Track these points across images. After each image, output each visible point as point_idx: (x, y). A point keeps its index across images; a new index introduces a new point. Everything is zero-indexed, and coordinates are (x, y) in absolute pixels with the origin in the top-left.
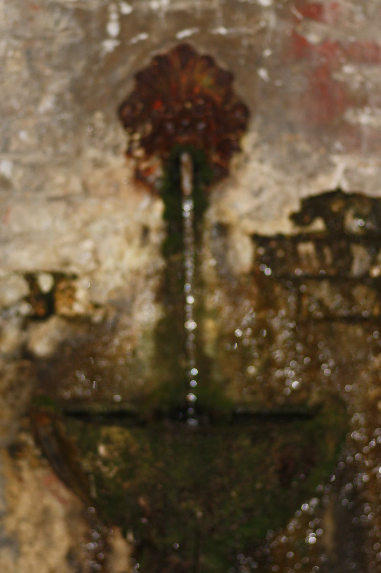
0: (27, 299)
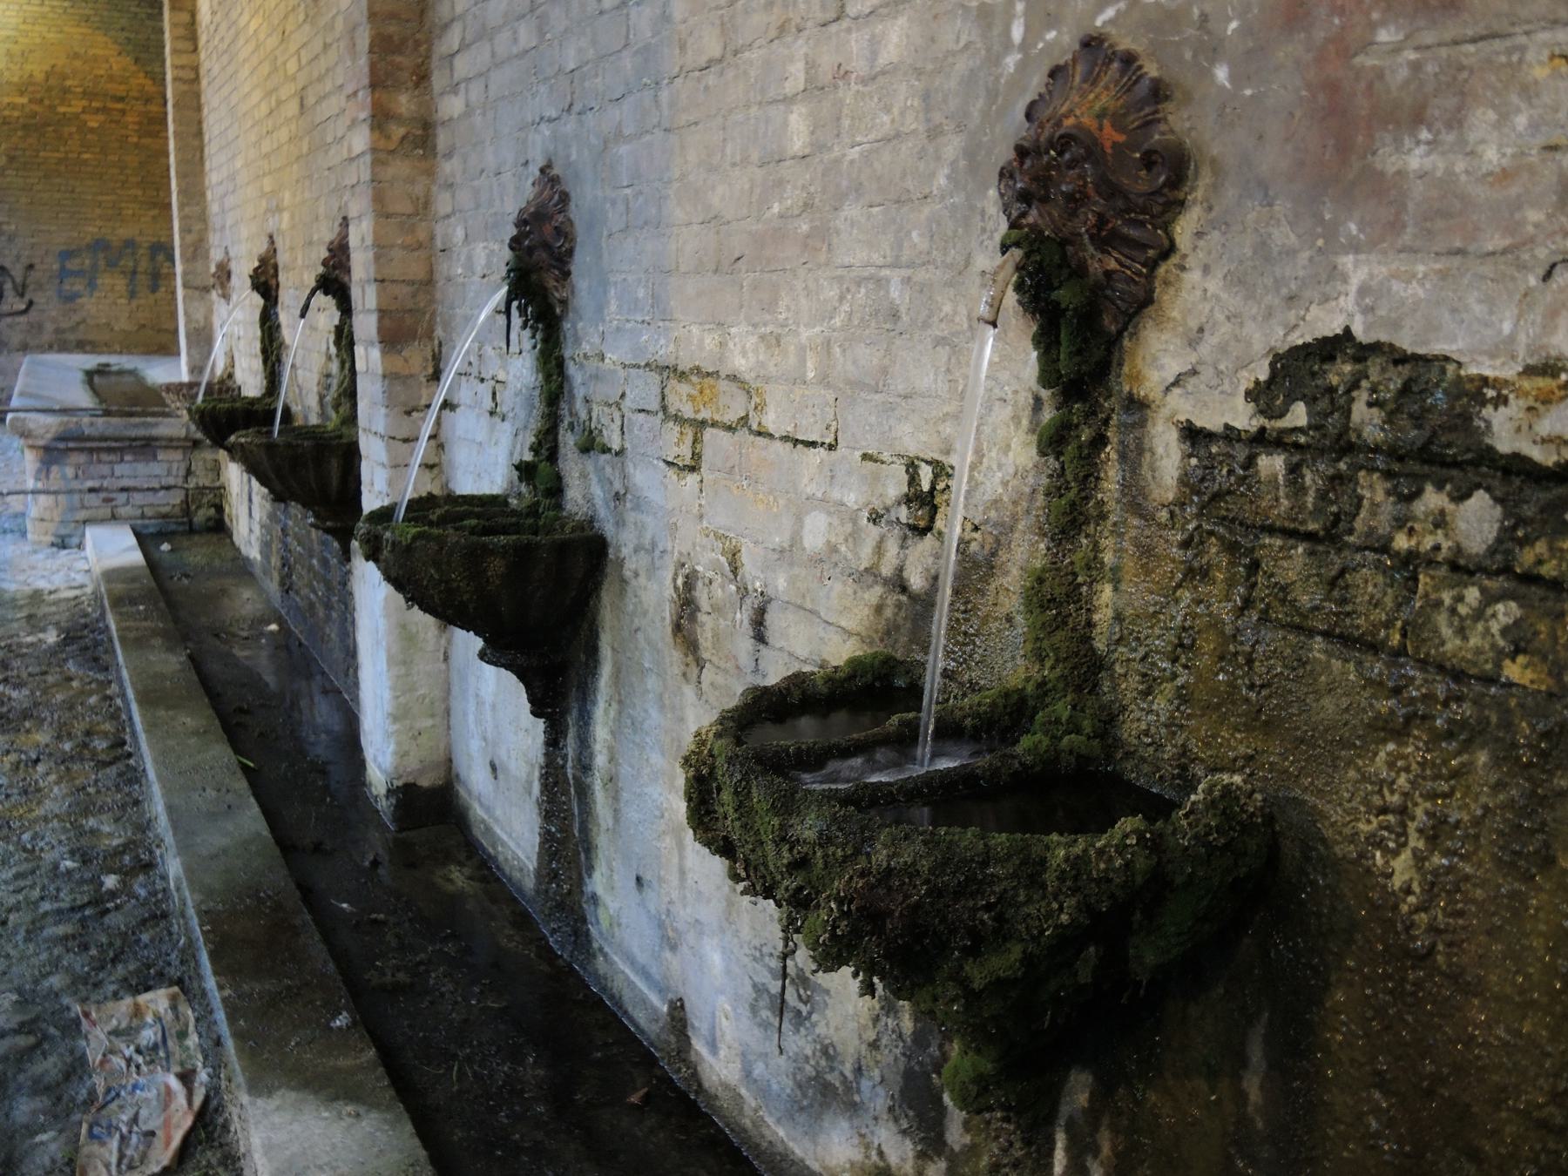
0: (908, 500)
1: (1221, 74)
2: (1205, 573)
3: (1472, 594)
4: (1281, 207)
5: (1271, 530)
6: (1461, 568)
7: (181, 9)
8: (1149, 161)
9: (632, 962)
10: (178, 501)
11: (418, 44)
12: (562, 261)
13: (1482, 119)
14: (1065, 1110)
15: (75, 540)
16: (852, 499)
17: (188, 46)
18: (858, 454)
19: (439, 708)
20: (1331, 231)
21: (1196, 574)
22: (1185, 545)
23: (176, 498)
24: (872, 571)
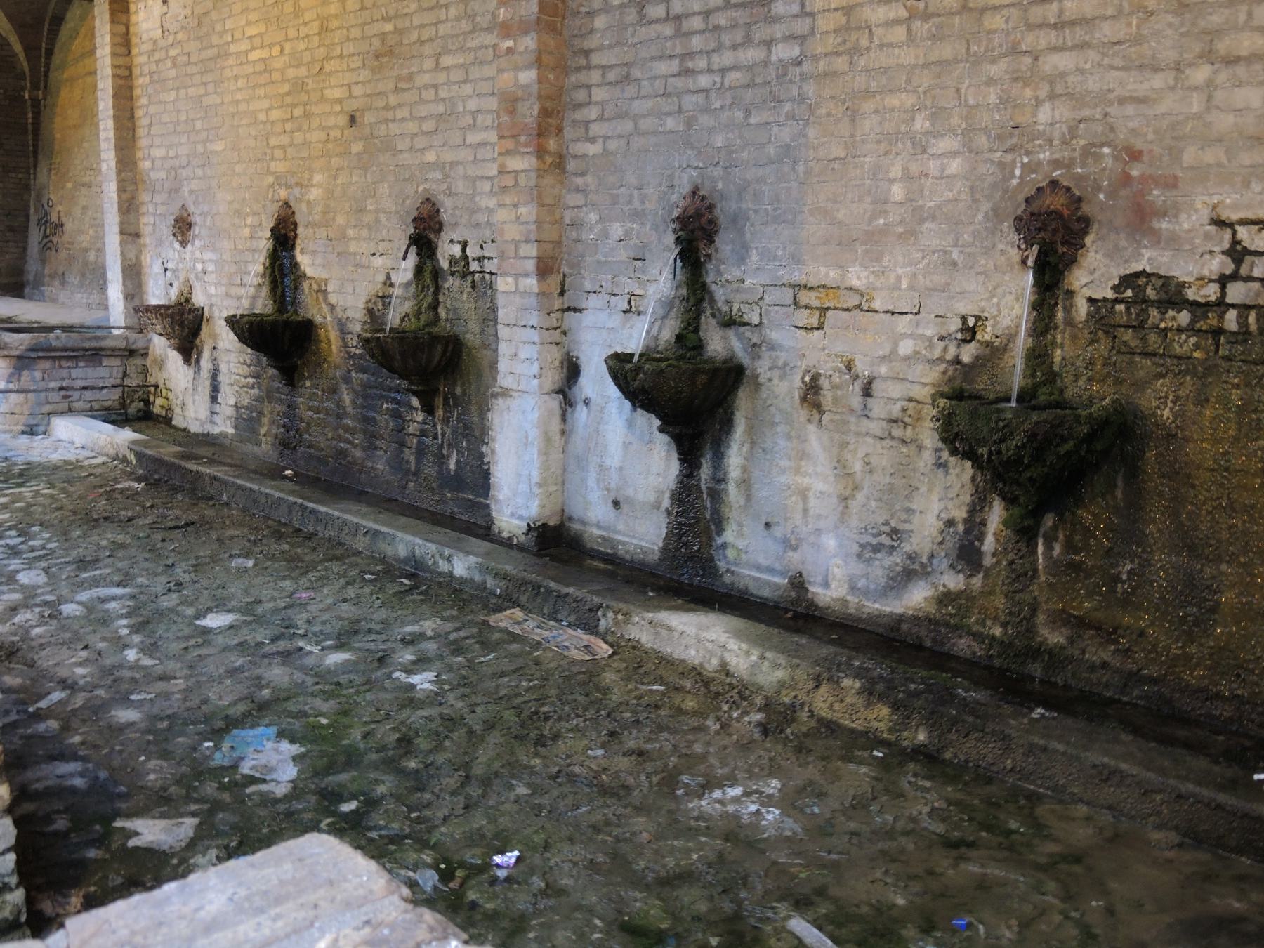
0: (962, 330)
1: (1102, 196)
2: (1097, 341)
3: (1184, 337)
4: (1122, 235)
5: (1120, 326)
6: (1180, 330)
8: (1079, 219)
9: (759, 568)
11: (559, 112)
13: (1183, 216)
14: (1042, 530)
15: (41, 429)
16: (929, 333)
17: (123, 50)
19: (560, 479)
20: (1139, 243)
21: (1092, 342)
23: (116, 394)
24: (941, 359)
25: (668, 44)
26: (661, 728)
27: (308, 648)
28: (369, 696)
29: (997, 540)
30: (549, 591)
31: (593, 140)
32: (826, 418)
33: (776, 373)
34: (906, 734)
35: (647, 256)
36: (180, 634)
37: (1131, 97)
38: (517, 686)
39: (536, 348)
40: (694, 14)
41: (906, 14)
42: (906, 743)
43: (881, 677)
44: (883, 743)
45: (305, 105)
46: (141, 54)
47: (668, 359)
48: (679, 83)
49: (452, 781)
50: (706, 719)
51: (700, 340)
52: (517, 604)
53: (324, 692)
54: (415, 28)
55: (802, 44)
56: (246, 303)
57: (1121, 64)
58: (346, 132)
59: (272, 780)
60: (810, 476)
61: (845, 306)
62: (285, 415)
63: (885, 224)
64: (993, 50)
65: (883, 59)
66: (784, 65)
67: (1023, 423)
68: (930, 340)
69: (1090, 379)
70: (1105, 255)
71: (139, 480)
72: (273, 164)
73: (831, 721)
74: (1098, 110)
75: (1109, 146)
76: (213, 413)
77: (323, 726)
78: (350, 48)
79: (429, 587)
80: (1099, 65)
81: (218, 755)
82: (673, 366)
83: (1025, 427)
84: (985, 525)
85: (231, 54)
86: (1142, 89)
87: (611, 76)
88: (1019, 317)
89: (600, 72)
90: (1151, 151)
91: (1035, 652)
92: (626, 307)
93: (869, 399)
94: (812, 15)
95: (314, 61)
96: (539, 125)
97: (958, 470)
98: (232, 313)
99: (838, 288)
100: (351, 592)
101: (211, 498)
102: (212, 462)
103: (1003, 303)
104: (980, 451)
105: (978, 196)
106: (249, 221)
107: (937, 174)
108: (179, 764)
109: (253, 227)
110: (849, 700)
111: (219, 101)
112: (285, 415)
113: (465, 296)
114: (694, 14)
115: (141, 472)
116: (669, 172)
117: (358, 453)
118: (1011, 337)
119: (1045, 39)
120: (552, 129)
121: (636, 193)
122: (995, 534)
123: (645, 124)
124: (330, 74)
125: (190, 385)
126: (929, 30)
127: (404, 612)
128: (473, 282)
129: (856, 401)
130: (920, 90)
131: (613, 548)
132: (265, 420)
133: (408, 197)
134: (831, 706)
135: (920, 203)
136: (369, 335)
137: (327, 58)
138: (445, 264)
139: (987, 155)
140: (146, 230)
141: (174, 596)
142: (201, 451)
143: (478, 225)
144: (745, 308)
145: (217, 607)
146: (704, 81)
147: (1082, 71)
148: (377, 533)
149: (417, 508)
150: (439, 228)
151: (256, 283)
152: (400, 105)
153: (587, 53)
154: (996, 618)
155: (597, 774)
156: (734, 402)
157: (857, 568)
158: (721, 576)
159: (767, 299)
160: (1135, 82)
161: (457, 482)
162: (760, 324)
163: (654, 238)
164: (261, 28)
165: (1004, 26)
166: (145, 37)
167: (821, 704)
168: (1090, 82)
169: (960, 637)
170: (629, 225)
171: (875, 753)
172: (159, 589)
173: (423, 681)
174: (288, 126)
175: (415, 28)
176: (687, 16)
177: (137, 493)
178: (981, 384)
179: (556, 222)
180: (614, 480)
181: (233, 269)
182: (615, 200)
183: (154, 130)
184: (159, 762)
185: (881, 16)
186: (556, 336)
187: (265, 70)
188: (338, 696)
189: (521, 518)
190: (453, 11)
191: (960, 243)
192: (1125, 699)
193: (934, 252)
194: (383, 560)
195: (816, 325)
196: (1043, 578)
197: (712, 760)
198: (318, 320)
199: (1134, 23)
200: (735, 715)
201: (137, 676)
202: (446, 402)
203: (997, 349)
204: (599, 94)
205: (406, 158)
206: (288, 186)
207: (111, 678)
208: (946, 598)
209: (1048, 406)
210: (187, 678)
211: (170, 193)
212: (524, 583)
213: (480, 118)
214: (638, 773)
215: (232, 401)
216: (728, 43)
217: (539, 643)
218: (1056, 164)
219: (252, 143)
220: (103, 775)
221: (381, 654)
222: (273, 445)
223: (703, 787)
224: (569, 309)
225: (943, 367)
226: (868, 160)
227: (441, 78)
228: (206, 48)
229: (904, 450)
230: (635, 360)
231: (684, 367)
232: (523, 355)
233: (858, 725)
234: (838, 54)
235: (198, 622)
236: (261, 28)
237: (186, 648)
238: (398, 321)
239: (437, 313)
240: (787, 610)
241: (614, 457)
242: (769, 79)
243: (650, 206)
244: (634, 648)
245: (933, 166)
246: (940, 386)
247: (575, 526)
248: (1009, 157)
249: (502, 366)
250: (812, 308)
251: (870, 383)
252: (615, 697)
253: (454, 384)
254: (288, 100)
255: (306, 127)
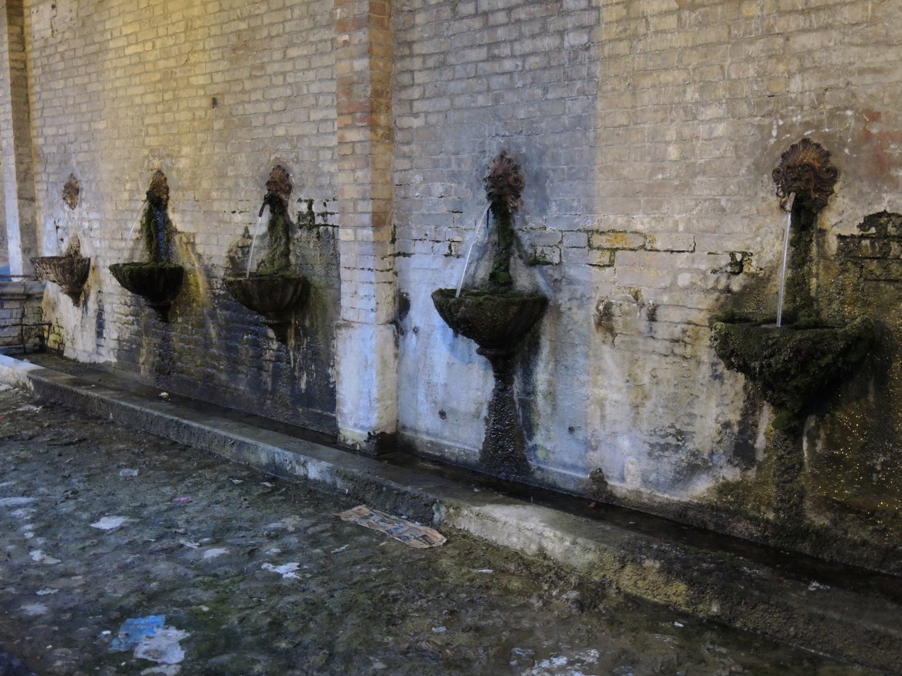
0: (731, 264)
1: (846, 151)
2: (847, 271)
4: (865, 183)
5: (866, 258)
7: (14, 25)
8: (828, 170)
9: (565, 466)
10: (16, 334)
11: (387, 93)
12: (516, 190)
14: (806, 430)
16: (703, 267)
17: (18, 47)
18: (706, 253)
21: (843, 271)
22: (841, 264)
23: (16, 332)
24: (714, 289)
25: (478, 35)
26: (493, 607)
27: (188, 545)
28: (242, 586)
29: (767, 438)
30: (390, 490)
31: (416, 115)
32: (618, 340)
33: (575, 303)
34: (701, 607)
35: (464, 209)
36: (78, 536)
37: (869, 69)
38: (367, 573)
39: (374, 287)
40: (499, 10)
41: (676, 6)
42: (701, 615)
43: (677, 558)
44: (682, 615)
45: (174, 90)
46: (34, 50)
47: (483, 294)
48: (488, 67)
49: (318, 659)
50: (530, 597)
51: (510, 277)
52: (364, 502)
53: (204, 583)
54: (266, 26)
55: (589, 33)
56: (126, 254)
57: (860, 41)
58: (209, 112)
59: (163, 663)
60: (606, 388)
61: (631, 247)
62: (161, 346)
63: (663, 179)
64: (750, 33)
65: (659, 43)
66: (575, 51)
67: (789, 341)
68: (704, 273)
69: (842, 303)
70: (852, 200)
71: (37, 404)
72: (147, 140)
73: (636, 596)
74: (842, 79)
75: (852, 109)
76: (98, 345)
77: (204, 613)
78: (211, 43)
79: (288, 488)
80: (841, 43)
81: (115, 642)
82: (490, 300)
83: (790, 344)
84: (757, 426)
85: (111, 50)
86: (878, 62)
87: (431, 62)
88: (781, 253)
89: (421, 59)
90: (887, 112)
91: (805, 533)
92: (447, 251)
93: (654, 324)
94: (597, 8)
95: (181, 54)
96: (372, 104)
97: (731, 381)
98: (114, 262)
99: (625, 232)
100: (222, 495)
101: (99, 418)
102: (99, 387)
103: (765, 242)
104: (753, 365)
105: (741, 153)
106: (128, 186)
107: (706, 136)
108: (82, 651)
109: (131, 191)
110: (650, 578)
111: (101, 88)
112: (161, 346)
113: (312, 245)
114: (499, 10)
115: (38, 397)
116: (481, 140)
117: (223, 377)
118: (773, 270)
119: (793, 23)
120: (383, 107)
121: (453, 158)
122: (765, 434)
123: (460, 101)
124: (195, 64)
125: (79, 323)
126: (696, 18)
127: (268, 511)
128: (318, 233)
129: (643, 325)
130: (690, 67)
131: (440, 451)
132: (143, 351)
133: (262, 165)
134: (636, 583)
135: (693, 160)
136: (232, 279)
137: (192, 51)
138: (294, 219)
139: (747, 120)
140: (40, 195)
141: (71, 503)
142: (88, 378)
143: (321, 187)
144: (547, 251)
145: (108, 511)
146: (508, 65)
147: (827, 49)
148: (242, 444)
149: (273, 421)
150: (289, 189)
151: (134, 237)
152: (254, 90)
153: (410, 44)
154: (769, 505)
155: (442, 648)
156: (540, 328)
157: (647, 464)
158: (533, 473)
159: (566, 242)
160: (872, 56)
161: (307, 399)
162: (561, 262)
163: (470, 194)
164: (135, 28)
165: (759, 13)
166: (37, 36)
167: (626, 582)
168: (834, 57)
169: (739, 521)
170: (449, 184)
171: (676, 624)
172: (58, 497)
173: (288, 570)
174: (160, 108)
175: (266, 26)
176: (493, 12)
177: (36, 415)
178: (749, 309)
179: (387, 183)
180: (440, 395)
181: (115, 226)
182: (436, 165)
183: (47, 113)
184: (64, 650)
185: (656, 8)
186: (389, 276)
187: (139, 62)
188: (216, 586)
189: (362, 428)
190: (297, 12)
191: (728, 191)
192: (884, 571)
193: (705, 201)
194: (248, 467)
195: (607, 263)
196: (808, 470)
197: (538, 633)
198: (188, 266)
199: (870, 7)
200: (554, 593)
201: (43, 574)
202: (297, 334)
203: (762, 279)
204: (420, 78)
205: (260, 133)
206: (161, 157)
207: (20, 576)
208: (725, 488)
209: (807, 327)
210: (85, 574)
211: (60, 164)
212: (368, 483)
213: (321, 99)
214: (477, 647)
215: (115, 336)
216: (527, 34)
217: (384, 535)
218: (807, 125)
219: (129, 122)
220: (16, 663)
221: (250, 548)
222: (150, 371)
223: (533, 658)
224: (399, 254)
225: (716, 295)
226: (647, 126)
227: (289, 66)
228: (90, 45)
229: (685, 364)
230: (457, 295)
231: (498, 301)
232: (361, 293)
233: (659, 600)
234: (620, 40)
235: (93, 525)
236: (135, 28)
237: (83, 548)
238: (255, 267)
239: (288, 260)
240: (590, 501)
241: (440, 374)
242: (562, 62)
243: (466, 168)
244: (464, 536)
245: (702, 130)
246: (714, 311)
247: (408, 434)
248: (767, 121)
249: (345, 302)
250: (603, 249)
251: (654, 310)
252: (452, 578)
253: (304, 318)
254: (160, 86)
255: (175, 109)
